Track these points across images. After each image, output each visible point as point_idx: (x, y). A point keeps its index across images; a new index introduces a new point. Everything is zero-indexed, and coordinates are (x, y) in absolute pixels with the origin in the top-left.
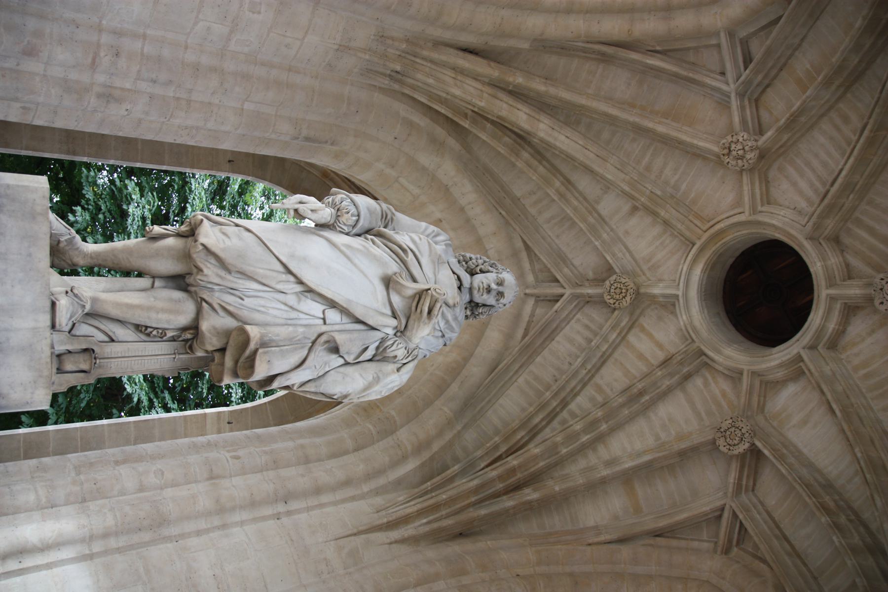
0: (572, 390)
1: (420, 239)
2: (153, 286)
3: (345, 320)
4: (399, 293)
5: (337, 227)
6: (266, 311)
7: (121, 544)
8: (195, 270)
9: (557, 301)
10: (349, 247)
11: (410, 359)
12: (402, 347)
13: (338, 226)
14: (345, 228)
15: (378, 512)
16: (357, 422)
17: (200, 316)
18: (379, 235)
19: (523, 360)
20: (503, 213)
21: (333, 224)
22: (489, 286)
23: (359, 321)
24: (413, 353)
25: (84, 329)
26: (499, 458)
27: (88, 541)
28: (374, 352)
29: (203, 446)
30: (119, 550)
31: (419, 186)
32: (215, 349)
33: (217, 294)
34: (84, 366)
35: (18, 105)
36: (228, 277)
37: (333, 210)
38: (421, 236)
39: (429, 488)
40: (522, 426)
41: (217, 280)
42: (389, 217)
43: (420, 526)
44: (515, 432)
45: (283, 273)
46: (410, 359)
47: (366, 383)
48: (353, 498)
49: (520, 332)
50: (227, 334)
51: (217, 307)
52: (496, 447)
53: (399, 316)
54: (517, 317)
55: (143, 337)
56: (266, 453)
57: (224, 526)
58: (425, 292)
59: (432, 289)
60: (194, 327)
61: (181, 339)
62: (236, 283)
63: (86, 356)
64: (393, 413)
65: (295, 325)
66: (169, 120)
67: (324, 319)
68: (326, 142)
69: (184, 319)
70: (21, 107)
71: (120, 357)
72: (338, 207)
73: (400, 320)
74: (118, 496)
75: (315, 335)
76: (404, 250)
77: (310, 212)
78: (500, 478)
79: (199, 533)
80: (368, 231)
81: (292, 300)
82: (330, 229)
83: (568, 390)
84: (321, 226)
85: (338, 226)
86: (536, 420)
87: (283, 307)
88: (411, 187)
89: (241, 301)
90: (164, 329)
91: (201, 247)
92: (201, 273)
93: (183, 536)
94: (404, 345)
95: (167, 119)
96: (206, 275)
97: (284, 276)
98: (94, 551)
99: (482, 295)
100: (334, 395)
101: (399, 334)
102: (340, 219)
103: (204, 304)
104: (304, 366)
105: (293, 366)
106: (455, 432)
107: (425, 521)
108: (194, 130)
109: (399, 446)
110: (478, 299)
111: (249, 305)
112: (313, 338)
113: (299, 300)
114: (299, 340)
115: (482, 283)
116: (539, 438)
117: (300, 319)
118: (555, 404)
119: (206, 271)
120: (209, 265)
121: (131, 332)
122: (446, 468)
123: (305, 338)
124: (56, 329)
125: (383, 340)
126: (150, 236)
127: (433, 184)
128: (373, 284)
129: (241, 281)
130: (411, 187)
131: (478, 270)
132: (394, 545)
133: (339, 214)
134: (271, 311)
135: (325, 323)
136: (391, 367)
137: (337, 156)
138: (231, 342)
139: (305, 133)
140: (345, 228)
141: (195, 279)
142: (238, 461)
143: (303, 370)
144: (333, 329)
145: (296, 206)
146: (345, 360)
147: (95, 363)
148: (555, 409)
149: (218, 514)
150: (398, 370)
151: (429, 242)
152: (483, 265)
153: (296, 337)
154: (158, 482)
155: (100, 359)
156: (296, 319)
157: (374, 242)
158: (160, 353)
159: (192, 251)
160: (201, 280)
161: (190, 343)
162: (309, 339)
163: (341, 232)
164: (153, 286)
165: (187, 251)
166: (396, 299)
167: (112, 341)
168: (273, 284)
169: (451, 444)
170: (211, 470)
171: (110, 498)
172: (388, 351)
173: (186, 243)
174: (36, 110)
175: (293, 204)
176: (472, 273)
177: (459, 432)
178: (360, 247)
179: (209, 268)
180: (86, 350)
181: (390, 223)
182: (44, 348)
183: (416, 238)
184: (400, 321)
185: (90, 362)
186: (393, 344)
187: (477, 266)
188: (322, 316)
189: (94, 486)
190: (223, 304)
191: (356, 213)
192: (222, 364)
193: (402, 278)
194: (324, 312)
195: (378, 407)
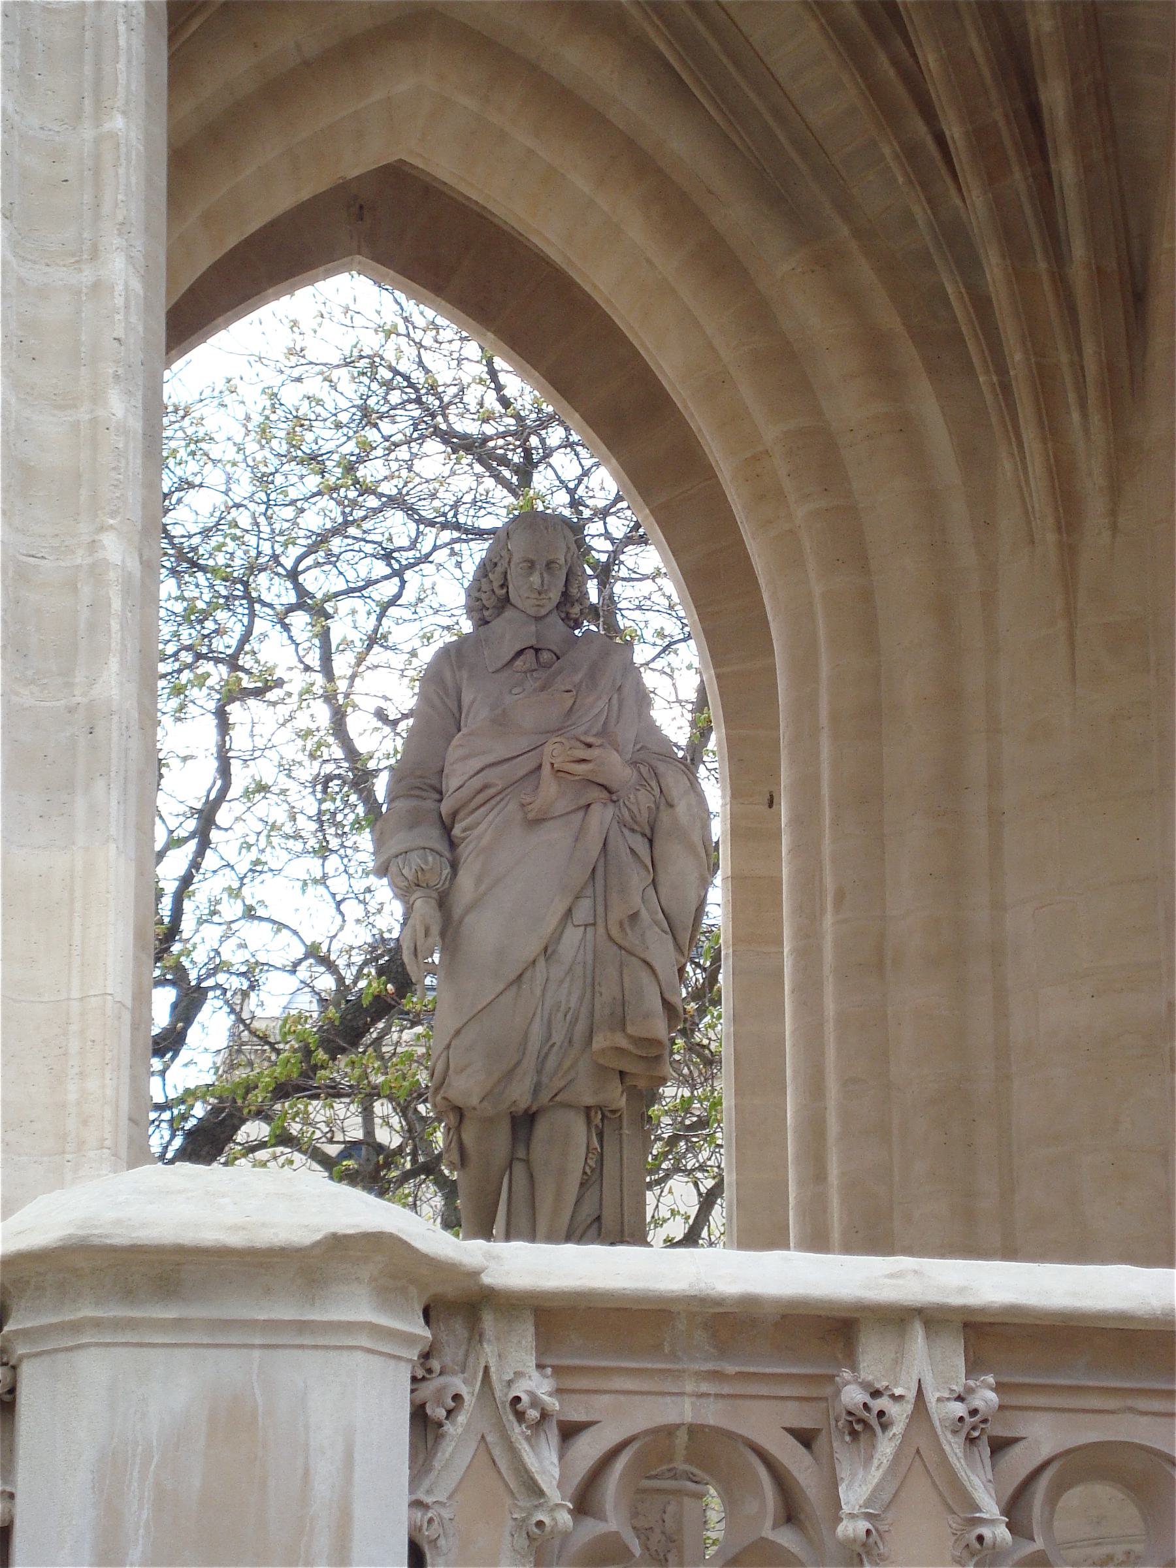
10: (479, 880)
11: (654, 784)
15: (1032, 542)
16: (791, 531)
39: (995, 379)
45: (519, 987)
67: (586, 926)
69: (579, 1128)
71: (622, 1210)
72: (413, 885)
75: (610, 944)
85: (444, 884)
89: (556, 1048)
91: (485, 1103)
100: (700, 896)
103: (558, 1099)
105: (653, 978)
106: (853, 245)
107: (1076, 416)
112: (615, 948)
125: (623, 824)
133: (425, 885)
136: (665, 817)
172: (639, 819)
186: (629, 810)
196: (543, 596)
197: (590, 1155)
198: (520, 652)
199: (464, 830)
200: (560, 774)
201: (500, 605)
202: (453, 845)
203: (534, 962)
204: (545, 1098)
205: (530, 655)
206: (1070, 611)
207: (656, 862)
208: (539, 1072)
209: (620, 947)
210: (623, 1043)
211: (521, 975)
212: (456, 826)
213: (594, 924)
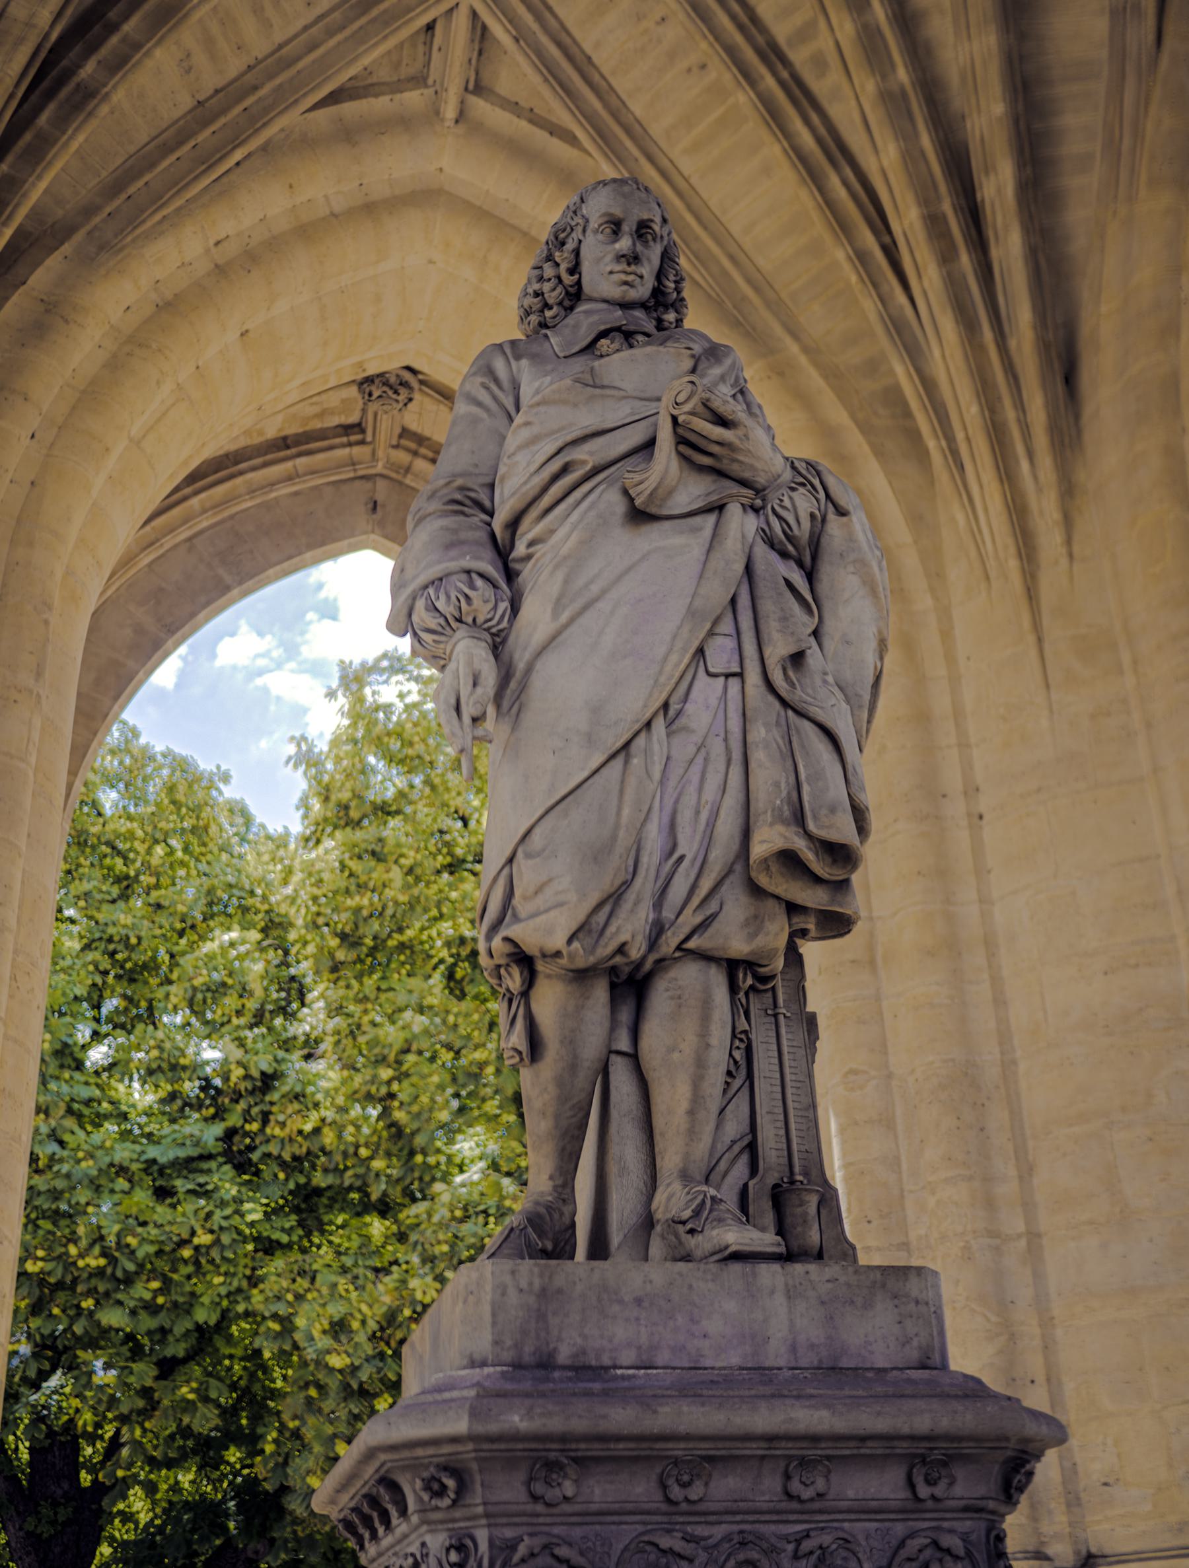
0: (741, 27)
1: (527, 424)
5: (501, 627)
6: (708, 807)
7: (1012, 1172)
9: (484, 28)
10: (558, 605)
11: (816, 482)
12: (791, 498)
13: (499, 623)
15: (988, 578)
17: (716, 954)
19: (636, 152)
20: (238, 155)
21: (493, 635)
22: (623, 256)
26: (891, 253)
27: (998, 1241)
30: (1026, 1171)
31: (158, 382)
37: (459, 634)
40: (815, 178)
42: (458, 496)
43: (1035, 477)
44: (830, 204)
45: (626, 762)
46: (816, 482)
48: (947, 635)
49: (557, 148)
52: (861, 258)
53: (720, 499)
54: (516, 150)
57: (990, 943)
58: (680, 431)
59: (675, 412)
67: (728, 676)
73: (730, 496)
74: (900, 1173)
75: (771, 698)
76: (565, 469)
77: (479, 690)
78: (946, 257)
79: (1000, 1001)
82: (504, 641)
83: (739, 39)
85: (499, 623)
86: (806, 139)
89: (686, 863)
91: (576, 945)
93: (1004, 1036)
94: (785, 491)
97: (635, 761)
98: (1022, 1228)
99: (641, 277)
103: (691, 944)
105: (835, 757)
106: (803, 360)
107: (1025, 465)
110: (643, 291)
115: (611, 272)
116: (856, 141)
118: (770, 82)
119: (623, 937)
120: (612, 929)
122: (893, 398)
127: (154, 346)
131: (568, 279)
132: (1076, 548)
133: (470, 620)
144: (756, 656)
145: (467, 719)
147: (802, 1182)
148: (782, 83)
149: (960, 954)
150: (842, 512)
155: (792, 1172)
156: (726, 740)
158: (775, 1047)
165: (571, 974)
169: (832, 375)
170: (853, 962)
171: (902, 1190)
172: (796, 531)
173: (549, 976)
177: (806, 350)
178: (560, 576)
179: (618, 929)
181: (472, 495)
182: (827, 1277)
185: (804, 1193)
186: (780, 517)
187: (559, 278)
188: (722, 679)
190: (696, 901)
193: (641, 483)
199: (531, 544)
201: (567, 303)
202: (510, 575)
203: (648, 725)
204: (670, 942)
206: (1036, 626)
208: (658, 905)
209: (784, 703)
210: (800, 844)
211: (627, 745)
212: (517, 543)
213: (740, 675)
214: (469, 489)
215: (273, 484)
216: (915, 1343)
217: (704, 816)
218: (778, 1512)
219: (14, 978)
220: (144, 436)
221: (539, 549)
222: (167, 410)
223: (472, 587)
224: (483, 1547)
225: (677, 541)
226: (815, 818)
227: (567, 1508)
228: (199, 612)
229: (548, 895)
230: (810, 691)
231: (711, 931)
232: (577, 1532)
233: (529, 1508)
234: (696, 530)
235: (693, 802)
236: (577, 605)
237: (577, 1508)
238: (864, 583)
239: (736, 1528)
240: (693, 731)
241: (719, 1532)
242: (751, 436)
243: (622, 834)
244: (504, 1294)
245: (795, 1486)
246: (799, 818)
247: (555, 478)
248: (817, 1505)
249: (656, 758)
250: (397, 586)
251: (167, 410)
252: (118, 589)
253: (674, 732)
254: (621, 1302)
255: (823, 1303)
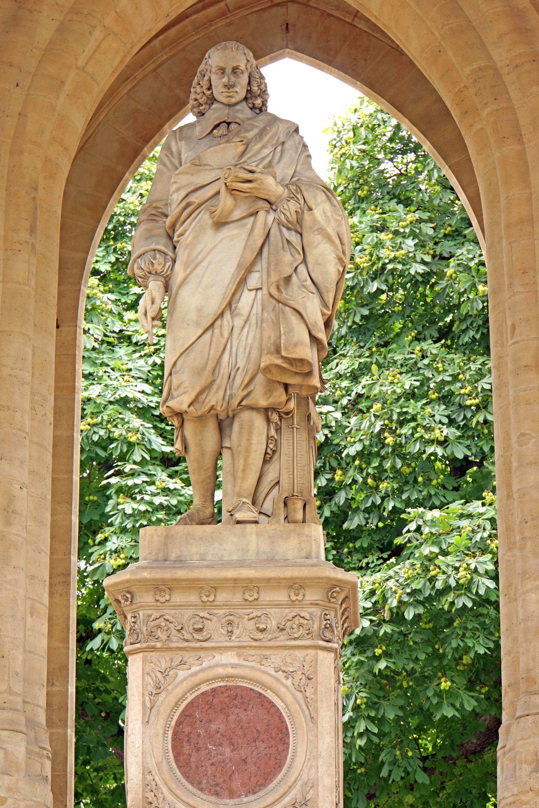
1: (175, 182)
2: (229, 448)
3: (258, 267)
4: (231, 212)
8: (213, 412)
14: (168, 264)
16: (482, 129)
17: (254, 406)
18: (173, 227)
21: (165, 278)
23: (260, 252)
24: (293, 191)
25: (268, 507)
28: (293, 233)
29: (499, 376)
32: (284, 393)
33: (234, 391)
34: (300, 505)
35: (29, 619)
36: (218, 382)
37: (150, 279)
38: (172, 181)
41: (221, 393)
45: (213, 332)
46: (299, 196)
47: (324, 241)
50: (271, 384)
51: (245, 393)
55: (276, 456)
56: (511, 285)
60: (266, 411)
61: (279, 423)
62: (223, 375)
63: (290, 503)
64: (467, 70)
65: (262, 320)
66: (27, 433)
67: (257, 289)
68: (34, 199)
69: (259, 421)
70: (31, 617)
75: (271, 299)
76: (188, 205)
77: (154, 306)
80: (170, 238)
81: (239, 322)
82: (170, 279)
84: (167, 288)
85: (166, 272)
87: (246, 329)
88: (92, 43)
90: (268, 438)
92: (215, 407)
94: (285, 201)
95: (26, 436)
96: (217, 403)
97: (216, 331)
99: (236, 92)
100: (339, 271)
101: (274, 207)
102: (158, 272)
103: (243, 403)
104: (301, 311)
105: (301, 321)
108: (36, 398)
109: (516, 66)
111: (244, 363)
113: (239, 314)
114: (275, 316)
115: (222, 92)
117: (257, 314)
119: (213, 403)
120: (207, 400)
121: (272, 467)
123: (274, 310)
124: (183, 454)
125: (280, 223)
126: (183, 452)
127: (85, 12)
128: (222, 239)
129: (222, 371)
130: (92, 43)
133: (154, 272)
134: (250, 341)
135: (261, 289)
136: (307, 216)
137: (52, 176)
138: (278, 379)
139: (24, 236)
140: (168, 264)
141: (221, 412)
142: (517, 327)
143: (306, 308)
145: (149, 319)
146: (301, 263)
151: (178, 174)
152: (202, 87)
153: (272, 320)
154: (533, 440)
157: (181, 235)
159: (196, 415)
160: (222, 407)
161: (283, 415)
162: (275, 306)
163: (172, 269)
164: (229, 448)
165: (195, 419)
166: (238, 214)
167: (278, 482)
168: (223, 341)
172: (291, 219)
173: (188, 420)
174: (33, 599)
175: (147, 322)
176: (212, 100)
178: (186, 253)
179: (210, 400)
180: (285, 504)
181: (160, 210)
183: (175, 187)
184: (262, 208)
187: (203, 92)
188: (254, 292)
189: (528, 524)
190: (243, 386)
191: (153, 252)
192: (301, 386)
194: (250, 290)
195: (460, 91)
196: (231, 90)
197: (270, 441)
198: (217, 126)
200: (233, 192)
205: (224, 126)
207: (306, 248)
209: (279, 302)
210: (279, 362)
211: (213, 324)
214: (159, 208)
215: (212, 21)
216: (305, 550)
217: (247, 350)
218: (243, 605)
219: (33, 409)
220: (86, 64)
221: (183, 238)
222: (100, 44)
223: (155, 259)
224: (141, 616)
225: (235, 232)
226: (286, 349)
227: (167, 604)
228: (165, 124)
229: (181, 390)
230: (290, 293)
231: (250, 397)
232: (173, 612)
233: (155, 604)
234: (244, 226)
235: (244, 344)
236: (193, 266)
237: (172, 604)
238: (325, 237)
239: (228, 610)
240: (242, 315)
241: (221, 612)
242: (264, 182)
243: (210, 362)
244: (152, 537)
245: (247, 596)
246: (278, 351)
247: (185, 209)
248: (255, 603)
249: (226, 328)
250: (267, 107)
251: (100, 44)
252: (107, 114)
253: (234, 316)
254: (194, 539)
255: (270, 537)
